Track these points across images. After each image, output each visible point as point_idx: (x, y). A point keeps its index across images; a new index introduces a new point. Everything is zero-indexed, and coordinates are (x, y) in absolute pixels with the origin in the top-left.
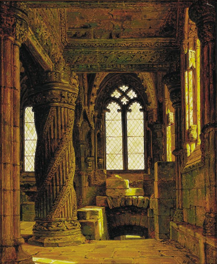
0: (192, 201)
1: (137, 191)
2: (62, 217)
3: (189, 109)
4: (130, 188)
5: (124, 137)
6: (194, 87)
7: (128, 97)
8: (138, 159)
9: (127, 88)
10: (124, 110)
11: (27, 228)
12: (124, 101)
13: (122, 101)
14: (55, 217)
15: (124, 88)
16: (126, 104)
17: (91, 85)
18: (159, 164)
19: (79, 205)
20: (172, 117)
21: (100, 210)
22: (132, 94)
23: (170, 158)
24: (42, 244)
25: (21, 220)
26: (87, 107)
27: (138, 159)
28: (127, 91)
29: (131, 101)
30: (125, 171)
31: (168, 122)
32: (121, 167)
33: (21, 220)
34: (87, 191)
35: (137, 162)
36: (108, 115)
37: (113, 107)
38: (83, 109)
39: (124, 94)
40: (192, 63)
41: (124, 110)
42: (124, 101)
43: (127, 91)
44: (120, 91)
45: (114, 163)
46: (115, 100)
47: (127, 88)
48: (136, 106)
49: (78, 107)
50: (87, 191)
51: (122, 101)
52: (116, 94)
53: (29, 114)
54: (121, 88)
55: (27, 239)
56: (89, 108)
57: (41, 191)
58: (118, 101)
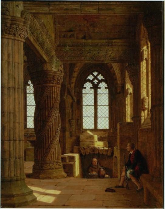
0: (111, 53)
1: (104, 144)
2: (52, 160)
3: (148, 102)
4: (98, 142)
5: (95, 110)
6: (147, 73)
7: (98, 79)
8: (102, 110)
9: (97, 73)
10: (96, 87)
11: (29, 167)
12: (96, 82)
13: (94, 82)
14: (48, 159)
15: (95, 73)
16: (96, 83)
17: (72, 72)
18: (120, 124)
19: (63, 153)
20: (131, 90)
21: (77, 156)
22: (100, 77)
23: (128, 120)
24: (39, 178)
25: (25, 160)
26: (69, 86)
27: (102, 110)
28: (98, 75)
29: (100, 81)
30: (95, 130)
31: (127, 93)
32: (93, 127)
33: (25, 160)
34: (69, 142)
35: (104, 124)
36: (84, 91)
37: (88, 85)
38: (67, 87)
39: (96, 78)
40: (145, 56)
41: (96, 87)
42: (96, 82)
43: (98, 75)
44: (93, 75)
45: (88, 123)
46: (89, 81)
47: (97, 73)
48: (103, 85)
49: (63, 86)
50: (69, 142)
51: (94, 82)
52: (91, 77)
53: (30, 89)
54: (94, 73)
55: (28, 176)
56: (71, 86)
57: (39, 140)
58: (92, 82)
